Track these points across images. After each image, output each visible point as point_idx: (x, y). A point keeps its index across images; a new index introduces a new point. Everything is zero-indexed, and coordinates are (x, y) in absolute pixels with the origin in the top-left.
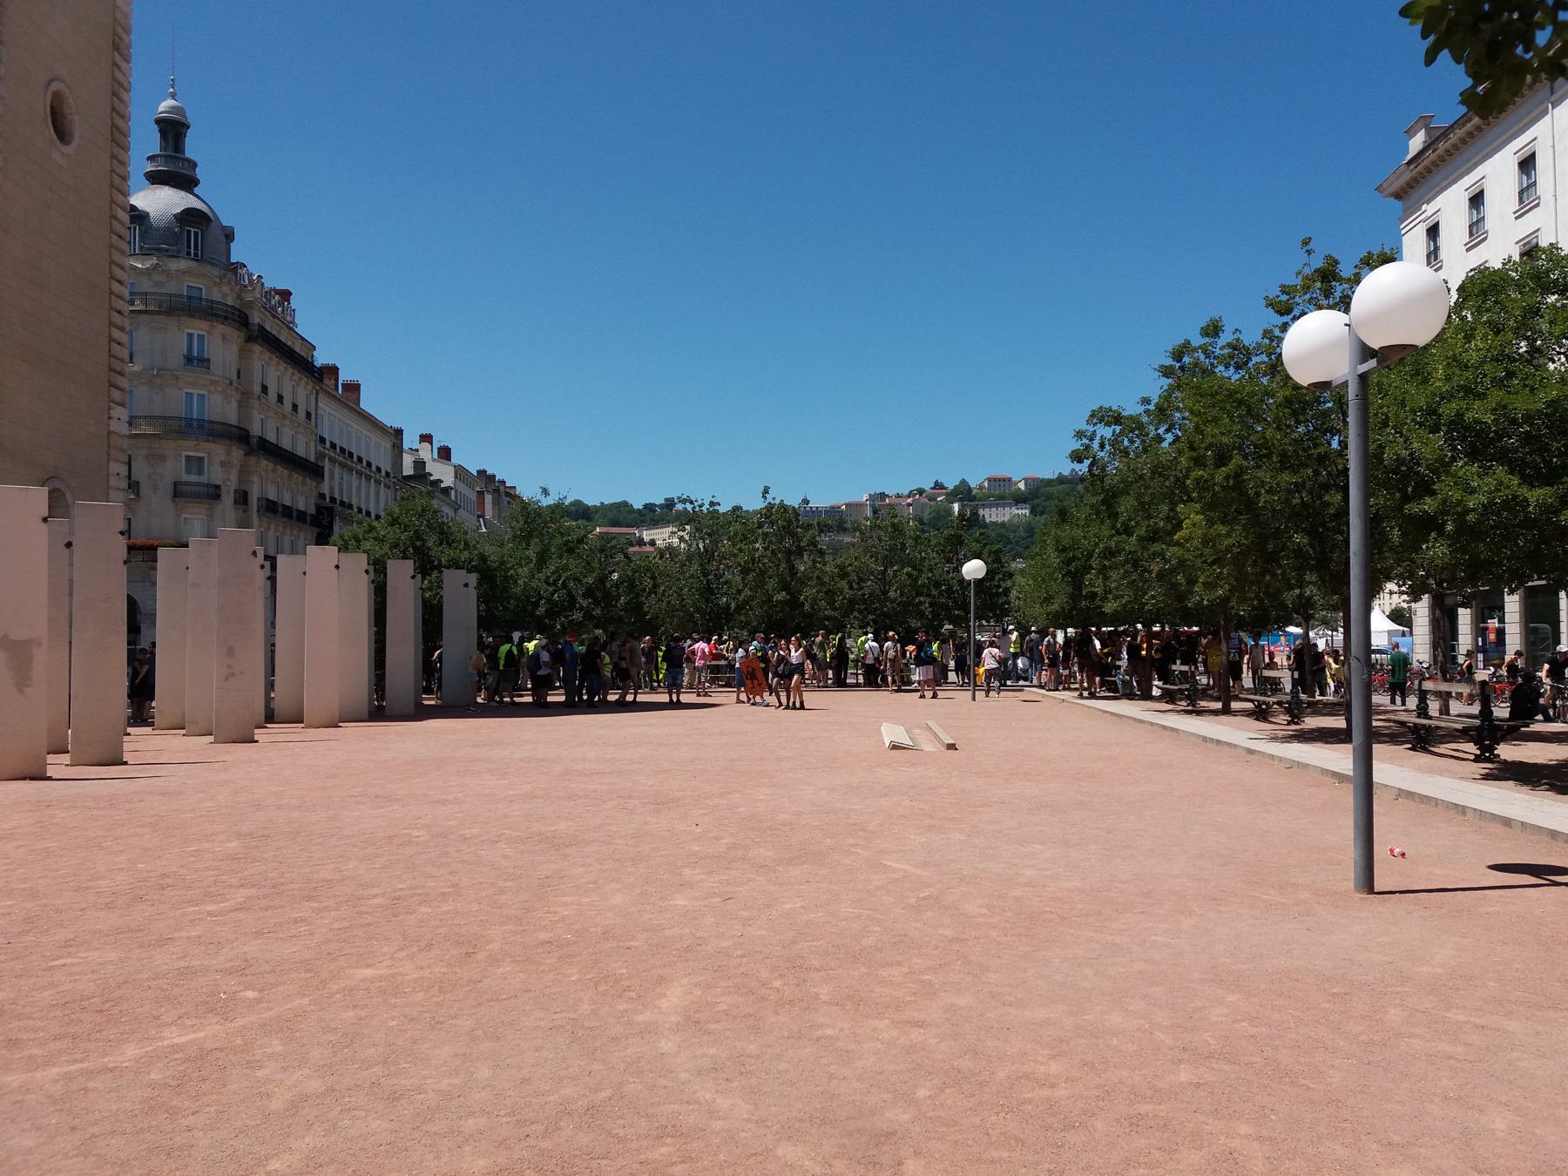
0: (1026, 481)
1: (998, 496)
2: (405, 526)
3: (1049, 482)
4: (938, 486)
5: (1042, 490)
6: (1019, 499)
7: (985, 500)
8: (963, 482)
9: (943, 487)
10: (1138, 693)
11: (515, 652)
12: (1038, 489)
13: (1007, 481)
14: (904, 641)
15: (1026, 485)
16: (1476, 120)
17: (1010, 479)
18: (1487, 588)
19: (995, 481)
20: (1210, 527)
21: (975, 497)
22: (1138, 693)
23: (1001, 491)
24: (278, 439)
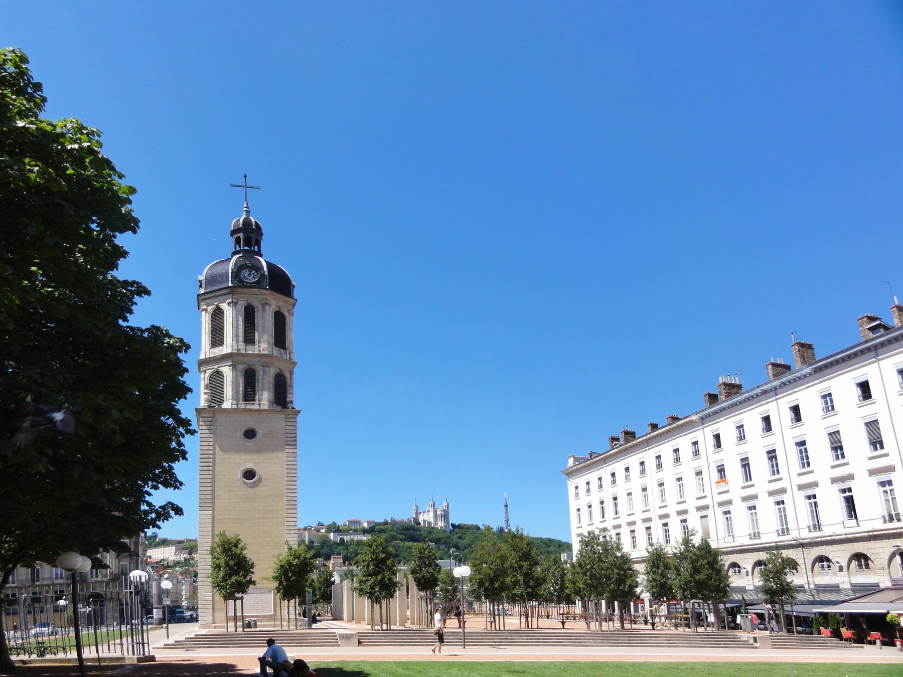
0: (368, 522)
1: (354, 530)
2: (447, 554)
3: (380, 524)
4: (321, 524)
5: (377, 527)
6: (365, 531)
7: (347, 532)
8: (334, 522)
9: (322, 525)
10: (34, 269)
11: (437, 616)
12: (374, 527)
13: (358, 522)
14: (317, 570)
15: (368, 524)
16: (141, 656)
17: (360, 522)
18: (35, 261)
19: (357, 522)
20: (625, 607)
21: (341, 530)
22: (34, 269)
23: (354, 527)
24: (507, 521)
